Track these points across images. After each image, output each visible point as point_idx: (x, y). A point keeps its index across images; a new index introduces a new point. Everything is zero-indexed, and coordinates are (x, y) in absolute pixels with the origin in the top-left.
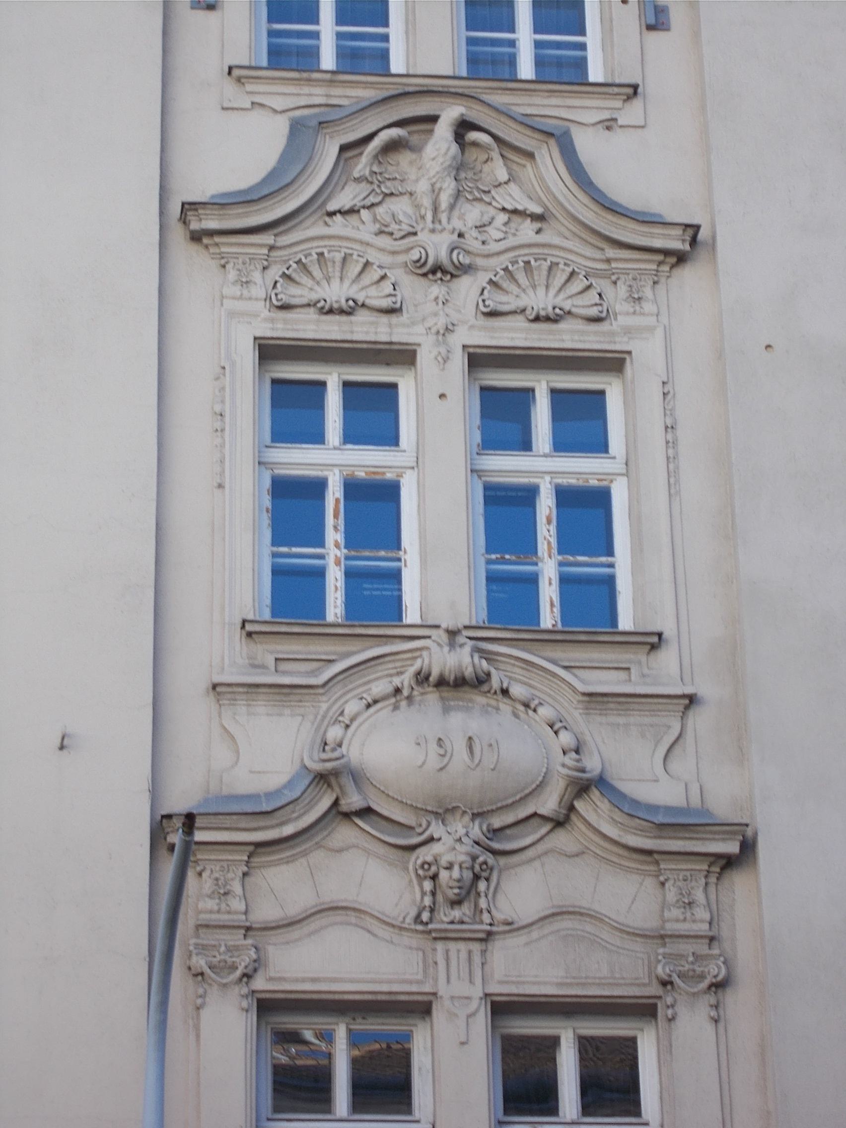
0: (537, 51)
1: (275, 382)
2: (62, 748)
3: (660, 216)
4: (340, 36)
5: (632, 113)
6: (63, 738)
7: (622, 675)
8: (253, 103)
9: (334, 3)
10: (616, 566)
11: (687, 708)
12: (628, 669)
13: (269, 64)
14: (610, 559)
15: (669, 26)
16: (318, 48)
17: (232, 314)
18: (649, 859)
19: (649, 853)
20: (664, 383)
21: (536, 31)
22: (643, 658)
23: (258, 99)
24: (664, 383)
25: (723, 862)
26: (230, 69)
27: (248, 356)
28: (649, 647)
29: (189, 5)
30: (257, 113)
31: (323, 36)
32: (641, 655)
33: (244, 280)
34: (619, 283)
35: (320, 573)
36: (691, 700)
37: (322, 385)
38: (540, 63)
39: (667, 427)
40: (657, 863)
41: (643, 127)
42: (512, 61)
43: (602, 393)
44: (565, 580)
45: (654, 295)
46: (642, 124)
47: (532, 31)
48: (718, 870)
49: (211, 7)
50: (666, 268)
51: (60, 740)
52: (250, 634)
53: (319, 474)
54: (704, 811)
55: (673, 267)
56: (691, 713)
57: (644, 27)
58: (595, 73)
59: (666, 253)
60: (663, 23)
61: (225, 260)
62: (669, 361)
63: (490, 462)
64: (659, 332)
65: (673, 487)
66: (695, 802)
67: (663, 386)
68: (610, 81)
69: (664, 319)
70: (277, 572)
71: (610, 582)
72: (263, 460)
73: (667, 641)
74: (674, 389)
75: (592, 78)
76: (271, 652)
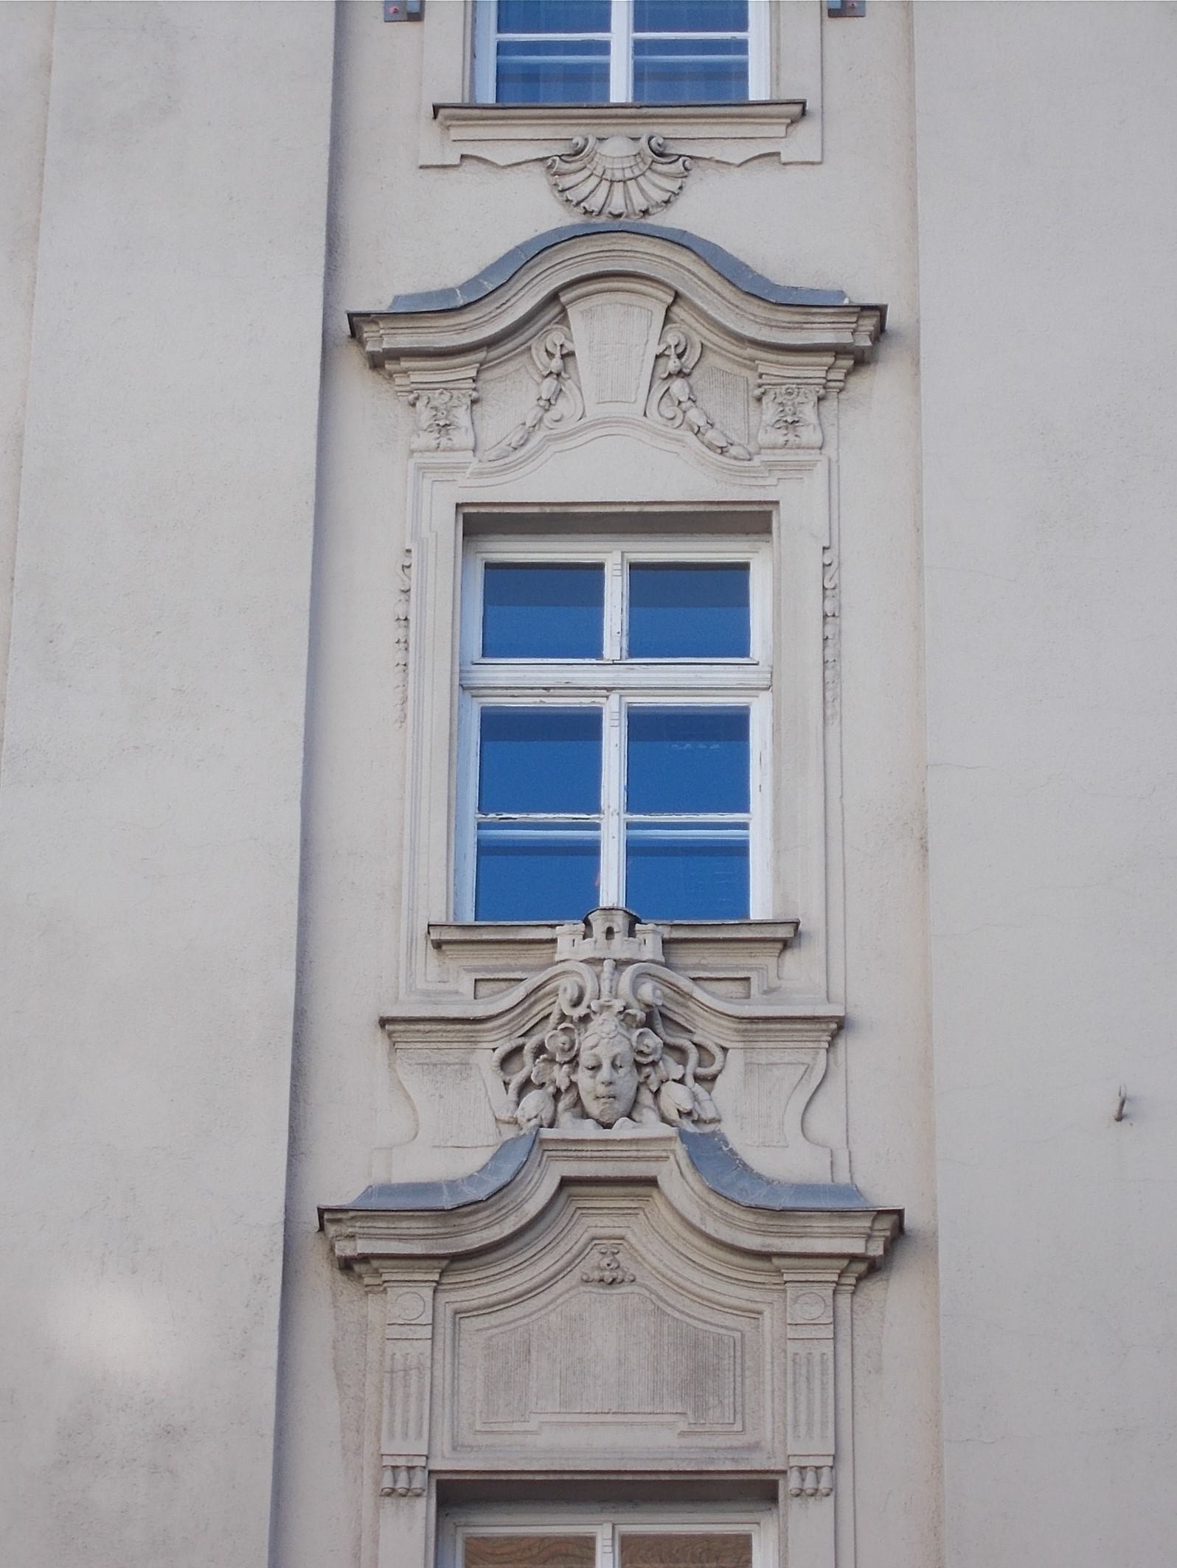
0: (637, 57)
1: (489, 566)
2: (1120, 1118)
3: (842, 294)
4: (639, 47)
5: (801, 142)
6: (1122, 1104)
7: (736, 988)
8: (463, 157)
9: (631, 4)
10: (751, 827)
11: (834, 1036)
12: (747, 979)
13: (635, 98)
14: (593, 817)
15: (864, 12)
16: (606, 67)
17: (422, 469)
18: (765, 1265)
19: (766, 1256)
20: (824, 548)
21: (638, 27)
22: (771, 962)
23: (469, 149)
24: (824, 548)
25: (861, 1267)
26: (436, 109)
27: (448, 529)
28: (780, 946)
29: (380, 12)
30: (469, 166)
31: (614, 49)
32: (766, 959)
33: (790, 419)
34: (765, 400)
35: (592, 850)
36: (839, 1027)
37: (597, 569)
38: (639, 75)
39: (825, 616)
40: (779, 1272)
41: (820, 163)
42: (602, 74)
43: (745, 567)
44: (635, 850)
45: (819, 415)
46: (818, 159)
47: (631, 27)
48: (853, 1281)
49: (416, 17)
50: (839, 375)
51: (1117, 1106)
52: (438, 945)
53: (586, 702)
54: (852, 1191)
55: (849, 374)
56: (841, 1043)
57: (826, 12)
58: (758, 88)
59: (838, 351)
60: (853, 7)
61: (762, 390)
62: (835, 516)
63: (480, 675)
64: (821, 470)
65: (829, 705)
66: (843, 1178)
67: (823, 553)
68: (775, 98)
69: (830, 451)
70: (485, 849)
71: (740, 850)
72: (466, 683)
73: (800, 934)
74: (839, 557)
75: (752, 97)
76: (468, 971)
